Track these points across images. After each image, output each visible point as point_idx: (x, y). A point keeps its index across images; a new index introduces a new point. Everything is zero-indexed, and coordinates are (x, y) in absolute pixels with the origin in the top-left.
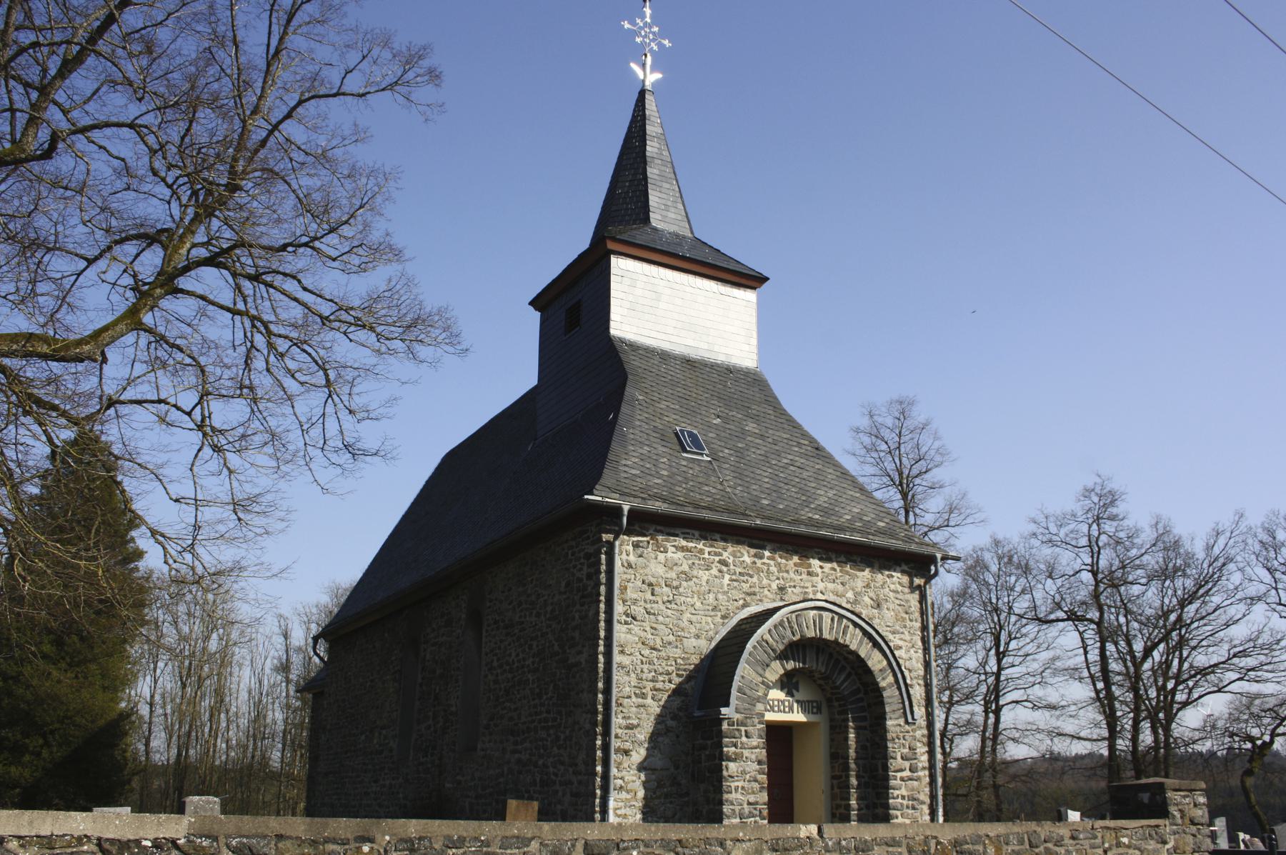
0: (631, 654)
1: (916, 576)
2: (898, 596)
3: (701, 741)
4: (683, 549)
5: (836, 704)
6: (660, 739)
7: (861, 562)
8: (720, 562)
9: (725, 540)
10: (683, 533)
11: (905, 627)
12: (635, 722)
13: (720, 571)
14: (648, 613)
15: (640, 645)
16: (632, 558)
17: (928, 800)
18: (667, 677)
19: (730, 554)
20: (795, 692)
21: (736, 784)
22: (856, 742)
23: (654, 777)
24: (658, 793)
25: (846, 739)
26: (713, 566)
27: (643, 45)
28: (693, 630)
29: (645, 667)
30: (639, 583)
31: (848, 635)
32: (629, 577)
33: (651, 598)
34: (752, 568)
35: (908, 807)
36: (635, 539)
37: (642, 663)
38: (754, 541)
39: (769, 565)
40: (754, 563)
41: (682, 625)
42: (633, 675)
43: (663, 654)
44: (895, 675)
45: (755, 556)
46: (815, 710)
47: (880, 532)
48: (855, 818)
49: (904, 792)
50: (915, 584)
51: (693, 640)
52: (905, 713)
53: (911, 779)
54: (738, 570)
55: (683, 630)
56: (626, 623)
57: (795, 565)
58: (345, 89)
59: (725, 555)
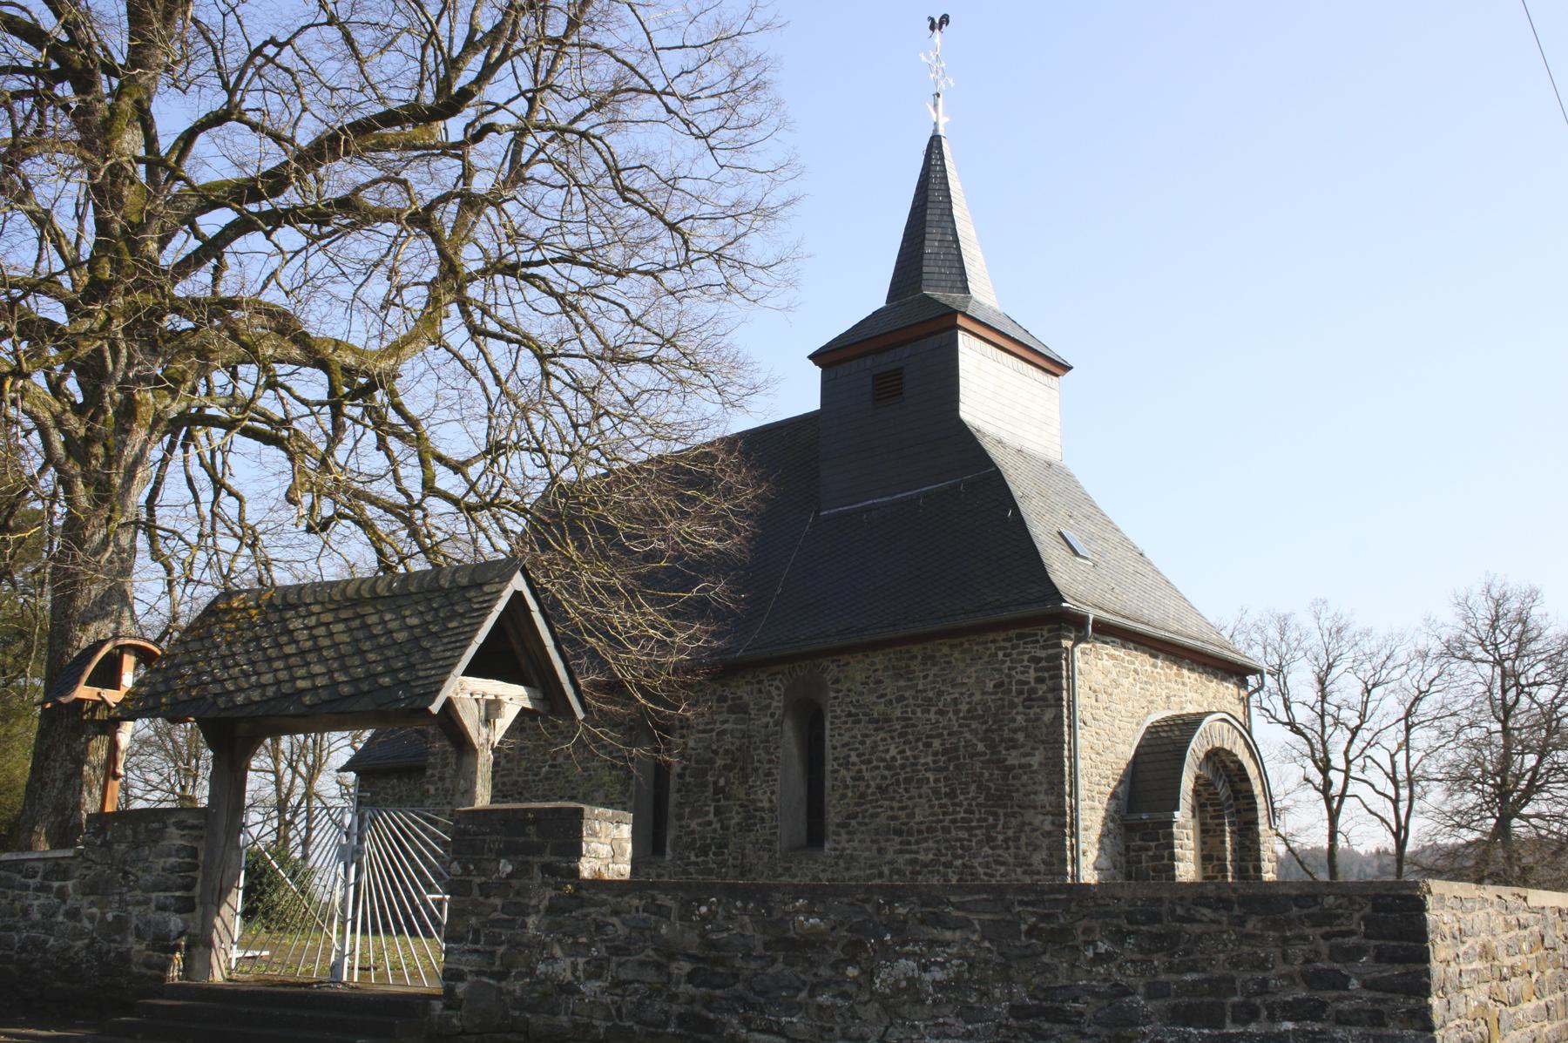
3: (1139, 843)
5: (1210, 809)
25: (1223, 842)
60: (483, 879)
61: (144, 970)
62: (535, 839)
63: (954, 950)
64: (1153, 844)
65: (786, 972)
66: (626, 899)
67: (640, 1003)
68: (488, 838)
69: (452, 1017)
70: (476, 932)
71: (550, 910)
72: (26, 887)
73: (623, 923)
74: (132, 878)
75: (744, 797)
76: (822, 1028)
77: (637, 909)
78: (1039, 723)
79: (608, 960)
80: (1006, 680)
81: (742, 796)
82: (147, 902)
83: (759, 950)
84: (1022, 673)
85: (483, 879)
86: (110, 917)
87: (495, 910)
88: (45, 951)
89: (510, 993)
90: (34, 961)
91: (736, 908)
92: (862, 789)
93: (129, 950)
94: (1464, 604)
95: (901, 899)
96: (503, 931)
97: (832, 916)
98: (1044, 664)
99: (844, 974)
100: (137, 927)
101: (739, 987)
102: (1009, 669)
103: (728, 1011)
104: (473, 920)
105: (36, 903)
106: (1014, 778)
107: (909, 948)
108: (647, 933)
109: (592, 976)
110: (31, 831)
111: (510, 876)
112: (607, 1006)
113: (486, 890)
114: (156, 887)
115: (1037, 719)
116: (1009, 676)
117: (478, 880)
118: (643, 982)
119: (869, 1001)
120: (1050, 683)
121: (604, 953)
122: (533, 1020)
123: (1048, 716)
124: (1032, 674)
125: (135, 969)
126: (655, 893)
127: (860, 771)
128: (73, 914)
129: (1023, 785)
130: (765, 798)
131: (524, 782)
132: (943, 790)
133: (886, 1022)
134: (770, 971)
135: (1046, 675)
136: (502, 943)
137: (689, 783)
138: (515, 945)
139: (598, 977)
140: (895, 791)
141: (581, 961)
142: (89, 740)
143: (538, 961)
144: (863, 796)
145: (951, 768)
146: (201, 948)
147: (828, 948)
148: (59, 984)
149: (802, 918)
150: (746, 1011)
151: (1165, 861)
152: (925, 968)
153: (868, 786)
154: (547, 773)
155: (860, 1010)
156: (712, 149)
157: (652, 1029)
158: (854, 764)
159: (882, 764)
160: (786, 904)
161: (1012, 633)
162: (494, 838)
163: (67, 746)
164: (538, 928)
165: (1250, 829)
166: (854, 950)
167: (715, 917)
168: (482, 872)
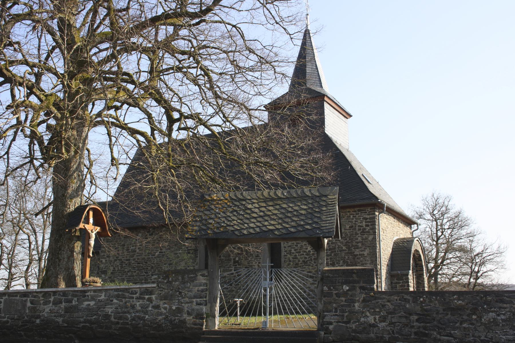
60: (337, 292)
61: (193, 326)
62: (356, 278)
63: (508, 310)
64: (401, 281)
65: (452, 318)
66: (392, 297)
67: (401, 329)
68: (337, 278)
69: (329, 336)
70: (336, 309)
71: (364, 301)
72: (133, 298)
73: (392, 304)
74: (183, 294)
75: (247, 264)
76: (466, 334)
77: (397, 300)
78: (366, 240)
79: (388, 316)
80: (354, 225)
81: (246, 264)
82: (191, 302)
83: (441, 311)
84: (360, 223)
85: (337, 292)
86: (174, 308)
87: (343, 302)
88: (144, 320)
89: (350, 328)
90: (139, 324)
91: (433, 299)
92: (297, 262)
93: (185, 319)
94: (425, 200)
95: (489, 295)
96: (346, 308)
97: (466, 301)
98: (368, 220)
99: (472, 318)
100: (188, 311)
101: (435, 323)
102: (355, 221)
103: (433, 330)
104: (334, 305)
105: (138, 303)
106: (357, 259)
107: (493, 309)
108: (401, 307)
109: (381, 322)
110: (57, 277)
111: (348, 290)
112: (388, 331)
113: (338, 295)
114: (195, 297)
115: (366, 239)
116: (355, 224)
117: (335, 292)
118: (401, 323)
119: (480, 326)
120: (371, 227)
121: (385, 314)
122: (360, 336)
123: (371, 238)
124: (364, 223)
125: (188, 326)
126: (403, 295)
127: (296, 255)
128: (157, 307)
129: (361, 261)
130: (256, 265)
131: (148, 258)
132: (329, 263)
133: (487, 331)
134: (446, 317)
135: (369, 224)
136: (347, 312)
137: (223, 259)
138: (351, 312)
139: (384, 321)
140: (310, 263)
141: (377, 317)
142: (74, 243)
143: (361, 317)
144: (297, 264)
145: (333, 255)
146: (210, 318)
147: (466, 310)
148: (153, 332)
149: (456, 301)
150: (439, 330)
151: (406, 287)
152: (498, 315)
153: (299, 261)
154: (158, 255)
155: (478, 328)
156: (291, 38)
157: (406, 337)
158: (293, 253)
159: (305, 253)
160: (450, 297)
161: (356, 209)
162: (340, 278)
163: (68, 245)
164: (359, 307)
165: (421, 277)
166: (474, 311)
167: (425, 302)
168: (336, 289)
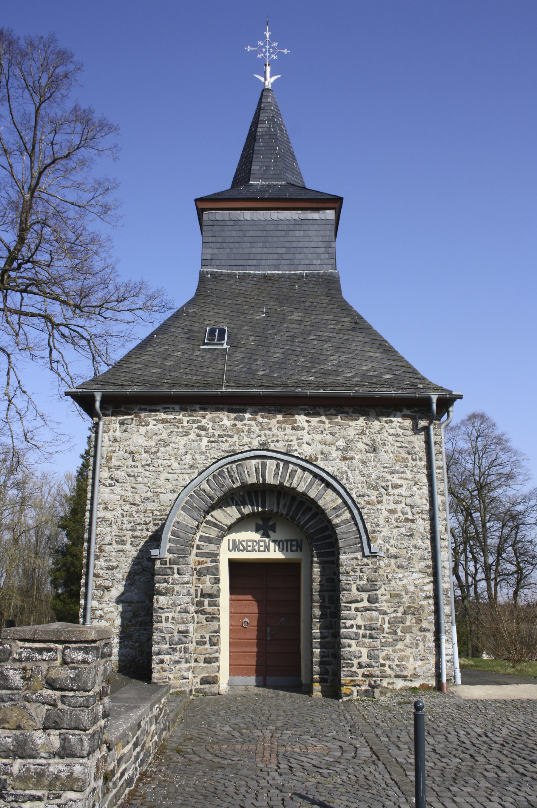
0: (113, 510)
1: (421, 418)
2: (399, 439)
4: (163, 421)
6: (137, 577)
7: (353, 412)
8: (198, 428)
9: (205, 410)
10: (163, 408)
11: (407, 466)
12: (115, 564)
13: (198, 435)
14: (129, 476)
15: (122, 502)
16: (118, 434)
17: (433, 628)
18: (145, 527)
19: (209, 420)
20: (270, 533)
21: (167, 615)
22: (321, 576)
23: (130, 608)
24: (133, 622)
26: (191, 432)
27: (263, 59)
28: (170, 486)
29: (125, 520)
30: (122, 453)
31: (296, 479)
32: (114, 448)
33: (133, 463)
34: (232, 430)
35: (364, 636)
36: (122, 418)
37: (123, 515)
38: (234, 407)
39: (249, 425)
40: (235, 425)
41: (159, 482)
42: (114, 526)
43: (141, 508)
44: (351, 512)
45: (235, 419)
46: (294, 548)
47: (388, 384)
48: (317, 645)
49: (359, 621)
50: (420, 426)
51: (169, 494)
52: (362, 547)
53: (369, 610)
54: (216, 433)
55: (159, 487)
56: (110, 485)
57: (278, 422)
58: (57, 155)
59: (204, 422)
